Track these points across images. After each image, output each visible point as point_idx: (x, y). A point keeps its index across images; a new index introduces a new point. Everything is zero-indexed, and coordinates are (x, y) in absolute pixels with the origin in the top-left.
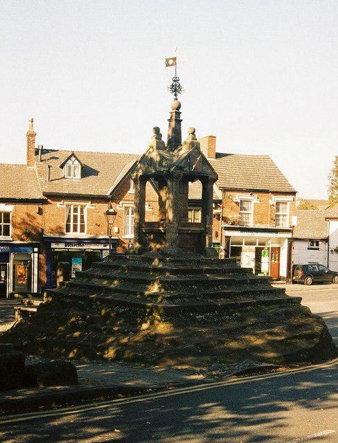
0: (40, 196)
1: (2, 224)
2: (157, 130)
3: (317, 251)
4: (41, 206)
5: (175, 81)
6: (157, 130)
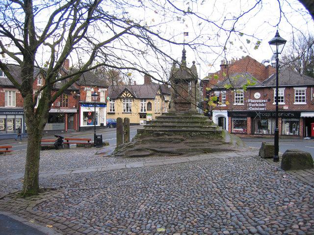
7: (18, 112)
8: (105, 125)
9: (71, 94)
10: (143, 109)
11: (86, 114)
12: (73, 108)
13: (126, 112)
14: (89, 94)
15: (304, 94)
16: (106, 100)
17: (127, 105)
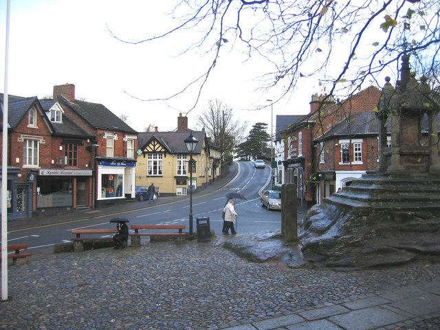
8: (133, 196)
9: (83, 145)
10: (182, 170)
11: (105, 177)
12: (84, 168)
13: (152, 175)
14: (110, 145)
16: (136, 155)
17: (155, 163)
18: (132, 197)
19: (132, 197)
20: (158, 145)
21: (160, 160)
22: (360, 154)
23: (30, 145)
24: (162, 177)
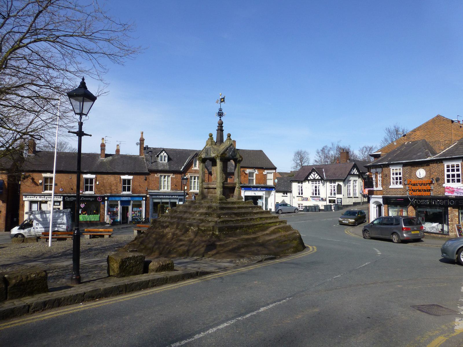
0: (147, 171)
1: (89, 185)
2: (211, 136)
3: (287, 197)
4: (147, 176)
5: (220, 110)
6: (211, 136)
7: (172, 195)
13: (314, 196)
15: (458, 170)
17: (316, 187)
18: (272, 211)
19: (272, 211)
20: (316, 175)
21: (319, 185)
22: (400, 178)
23: (195, 179)
24: (287, 196)
